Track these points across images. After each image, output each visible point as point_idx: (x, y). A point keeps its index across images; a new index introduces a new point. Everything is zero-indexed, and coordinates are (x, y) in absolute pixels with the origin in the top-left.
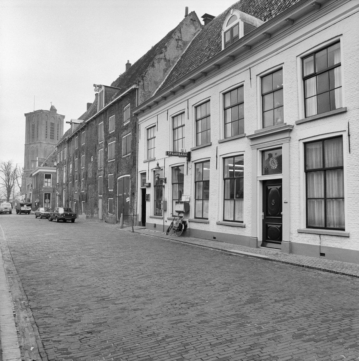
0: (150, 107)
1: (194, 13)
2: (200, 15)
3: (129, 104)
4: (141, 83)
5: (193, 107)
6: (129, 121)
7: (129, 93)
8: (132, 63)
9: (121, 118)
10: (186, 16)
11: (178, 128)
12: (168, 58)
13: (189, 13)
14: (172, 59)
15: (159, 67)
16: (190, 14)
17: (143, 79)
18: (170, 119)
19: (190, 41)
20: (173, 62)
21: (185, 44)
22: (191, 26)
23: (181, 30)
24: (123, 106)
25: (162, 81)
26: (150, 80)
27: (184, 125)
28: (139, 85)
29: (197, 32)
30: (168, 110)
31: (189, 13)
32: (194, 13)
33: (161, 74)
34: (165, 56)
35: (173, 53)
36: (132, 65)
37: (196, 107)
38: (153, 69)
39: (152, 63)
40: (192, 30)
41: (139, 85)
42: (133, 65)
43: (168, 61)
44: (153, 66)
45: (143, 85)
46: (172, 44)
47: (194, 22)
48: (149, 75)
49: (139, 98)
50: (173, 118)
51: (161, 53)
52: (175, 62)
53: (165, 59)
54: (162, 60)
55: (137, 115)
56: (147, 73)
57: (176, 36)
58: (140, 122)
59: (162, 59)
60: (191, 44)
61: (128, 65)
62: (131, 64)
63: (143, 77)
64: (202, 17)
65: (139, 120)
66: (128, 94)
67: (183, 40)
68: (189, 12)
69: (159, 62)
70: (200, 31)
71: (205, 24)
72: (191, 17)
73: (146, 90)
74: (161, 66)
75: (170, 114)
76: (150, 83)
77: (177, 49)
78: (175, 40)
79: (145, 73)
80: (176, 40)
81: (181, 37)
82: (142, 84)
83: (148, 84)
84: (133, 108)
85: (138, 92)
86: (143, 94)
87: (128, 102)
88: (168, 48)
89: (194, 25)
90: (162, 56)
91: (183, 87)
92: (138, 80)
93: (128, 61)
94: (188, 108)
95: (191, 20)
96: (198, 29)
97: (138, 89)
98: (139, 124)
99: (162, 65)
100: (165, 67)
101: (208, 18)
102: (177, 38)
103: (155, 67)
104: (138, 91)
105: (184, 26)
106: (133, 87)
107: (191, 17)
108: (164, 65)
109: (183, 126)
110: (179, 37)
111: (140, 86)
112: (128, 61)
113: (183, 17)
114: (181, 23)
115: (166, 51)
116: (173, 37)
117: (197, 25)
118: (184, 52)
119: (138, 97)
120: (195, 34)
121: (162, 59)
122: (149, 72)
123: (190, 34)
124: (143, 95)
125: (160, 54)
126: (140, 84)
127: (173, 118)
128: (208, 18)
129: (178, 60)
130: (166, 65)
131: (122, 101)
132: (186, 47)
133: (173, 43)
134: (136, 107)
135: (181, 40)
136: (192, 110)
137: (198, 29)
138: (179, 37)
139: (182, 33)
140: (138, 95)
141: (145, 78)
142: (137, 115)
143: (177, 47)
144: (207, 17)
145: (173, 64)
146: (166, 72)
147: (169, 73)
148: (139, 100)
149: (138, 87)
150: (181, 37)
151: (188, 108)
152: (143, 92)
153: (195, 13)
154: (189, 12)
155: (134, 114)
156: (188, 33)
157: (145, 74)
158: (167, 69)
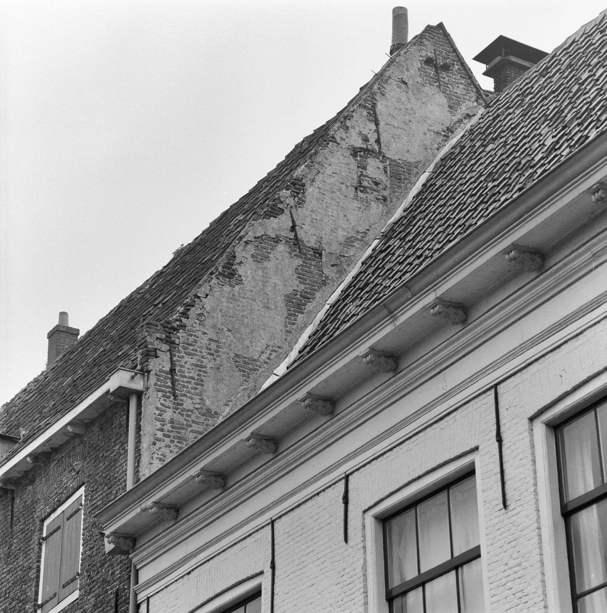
0: (220, 479)
1: (437, 33)
2: (470, 44)
3: (82, 491)
4: (160, 364)
5: (540, 428)
6: (76, 595)
7: (78, 431)
8: (84, 322)
9: (23, 580)
10: (398, 46)
11: (422, 582)
12: (308, 236)
13: (410, 37)
14: (335, 248)
15: (265, 283)
16: (419, 38)
17: (169, 342)
18: (366, 531)
19: (428, 161)
20: (340, 265)
21: (400, 173)
22: (429, 90)
23: (374, 106)
24: (41, 509)
25: (280, 359)
26: (213, 346)
27: (474, 555)
28: (145, 372)
29: (460, 121)
30: (347, 478)
31: (410, 37)
32: (437, 33)
33: (276, 320)
34: (293, 229)
35: (336, 214)
36: (82, 333)
37: (557, 427)
38: (227, 288)
39: (222, 261)
40: (434, 109)
41: (145, 372)
42: (89, 333)
43: (310, 256)
44: (230, 274)
45: (172, 371)
46: (329, 171)
47: (444, 74)
48: (209, 322)
49: (145, 444)
50: (385, 520)
51: (275, 212)
52: (350, 262)
53: (296, 243)
54: (281, 247)
55: (130, 540)
56: (193, 312)
57: (353, 133)
58: (149, 584)
59: (277, 240)
60: (436, 174)
61: (60, 334)
62: (77, 332)
63: (170, 330)
64: (478, 58)
65: (144, 576)
66: (75, 436)
67: (389, 155)
68: (414, 29)
69: (260, 258)
70: (478, 116)
71: (499, 87)
72: (428, 51)
73: (188, 404)
74: (275, 280)
75: (358, 503)
76: (209, 364)
77: (356, 198)
78: (348, 154)
79: (181, 309)
80: (355, 152)
81: (378, 141)
82: (167, 368)
83: (200, 366)
84: (107, 498)
85: (139, 414)
86: (172, 421)
87: (72, 484)
88: (310, 190)
89: (443, 88)
90: (278, 225)
91: (459, 311)
92: (144, 344)
93: (63, 315)
94: (500, 440)
95: (429, 61)
96: (463, 109)
97: (139, 395)
98: (141, 597)
99: (280, 273)
100: (295, 285)
101: (513, 59)
102: (359, 143)
103: (240, 282)
104: (139, 406)
105: (393, 90)
106: (118, 380)
107: (426, 53)
108: (289, 273)
109: (456, 565)
110: (366, 140)
111: (153, 379)
112: (63, 315)
113: (382, 58)
114: (380, 77)
115: (301, 203)
116: (333, 139)
117: (460, 90)
118: (398, 213)
119: (138, 442)
120: (450, 130)
121: (277, 240)
122: (208, 303)
123: (422, 127)
124: (168, 427)
125: (268, 215)
126: (153, 364)
127: (385, 520)
128: (513, 59)
129: (369, 251)
130: (301, 274)
131: (32, 482)
132: (407, 190)
133: (336, 164)
134: (129, 487)
135: (379, 154)
136: (529, 452)
137: (463, 109)
138: (366, 140)
139: (382, 124)
140: (138, 428)
141: (181, 334)
142: (130, 540)
143: (359, 187)
144: (505, 55)
145: (342, 273)
146: (300, 308)
147: (321, 315)
148: (148, 449)
149: (138, 385)
150: (378, 141)
151: (500, 440)
152: (168, 415)
153: (447, 36)
154: (414, 29)
155: (114, 533)
156: (414, 125)
157: (185, 314)
158: (307, 297)
